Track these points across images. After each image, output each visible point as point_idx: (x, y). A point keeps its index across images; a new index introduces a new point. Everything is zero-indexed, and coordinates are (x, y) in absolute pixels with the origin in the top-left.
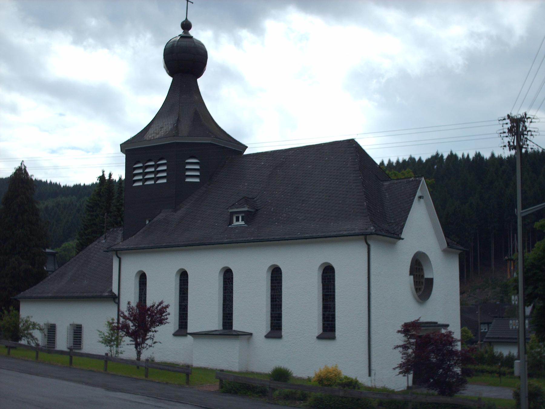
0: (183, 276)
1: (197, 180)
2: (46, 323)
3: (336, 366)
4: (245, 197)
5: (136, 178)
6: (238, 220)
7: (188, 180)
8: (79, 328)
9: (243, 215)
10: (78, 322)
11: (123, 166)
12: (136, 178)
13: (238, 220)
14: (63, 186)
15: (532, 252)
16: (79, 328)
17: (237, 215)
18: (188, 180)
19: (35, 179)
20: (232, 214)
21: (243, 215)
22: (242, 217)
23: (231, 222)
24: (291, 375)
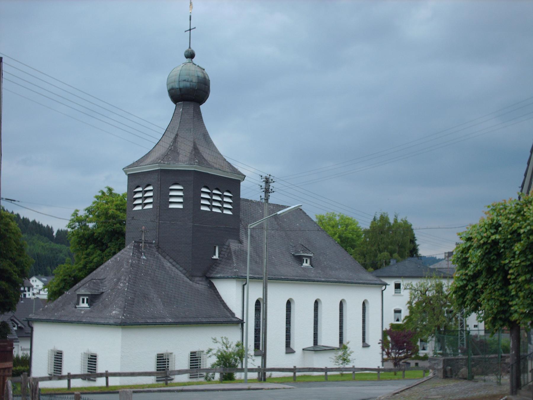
0: (289, 303)
1: (181, 206)
2: (85, 352)
3: (380, 353)
4: (92, 279)
5: (137, 202)
6: (83, 302)
7: (171, 206)
8: (60, 353)
9: (88, 297)
10: (93, 351)
11: (162, 134)
12: (137, 202)
13: (83, 302)
14: (59, 232)
15: (452, 265)
16: (60, 353)
17: (83, 297)
18: (171, 206)
19: (23, 218)
20: (79, 296)
21: (88, 297)
22: (87, 299)
23: (78, 303)
24: (27, 358)
